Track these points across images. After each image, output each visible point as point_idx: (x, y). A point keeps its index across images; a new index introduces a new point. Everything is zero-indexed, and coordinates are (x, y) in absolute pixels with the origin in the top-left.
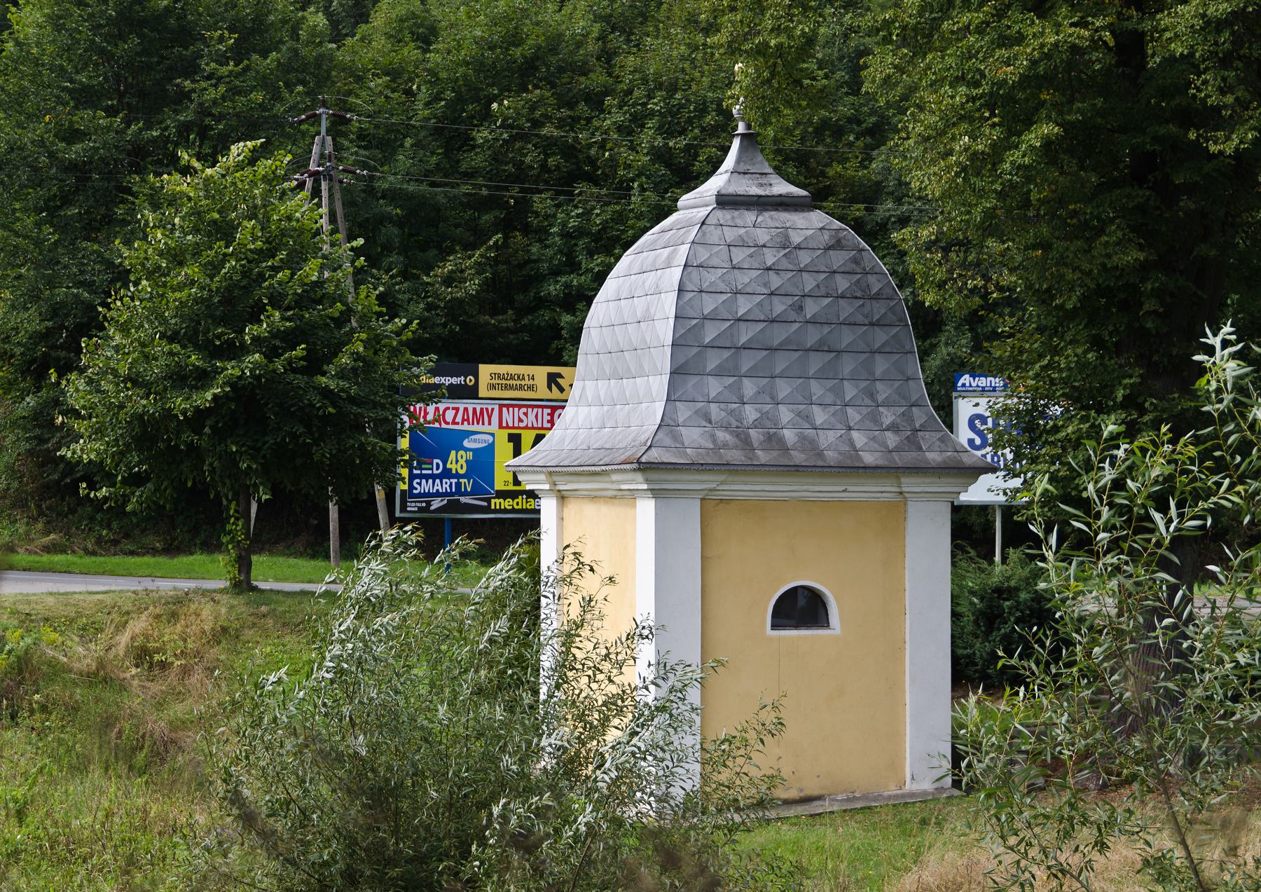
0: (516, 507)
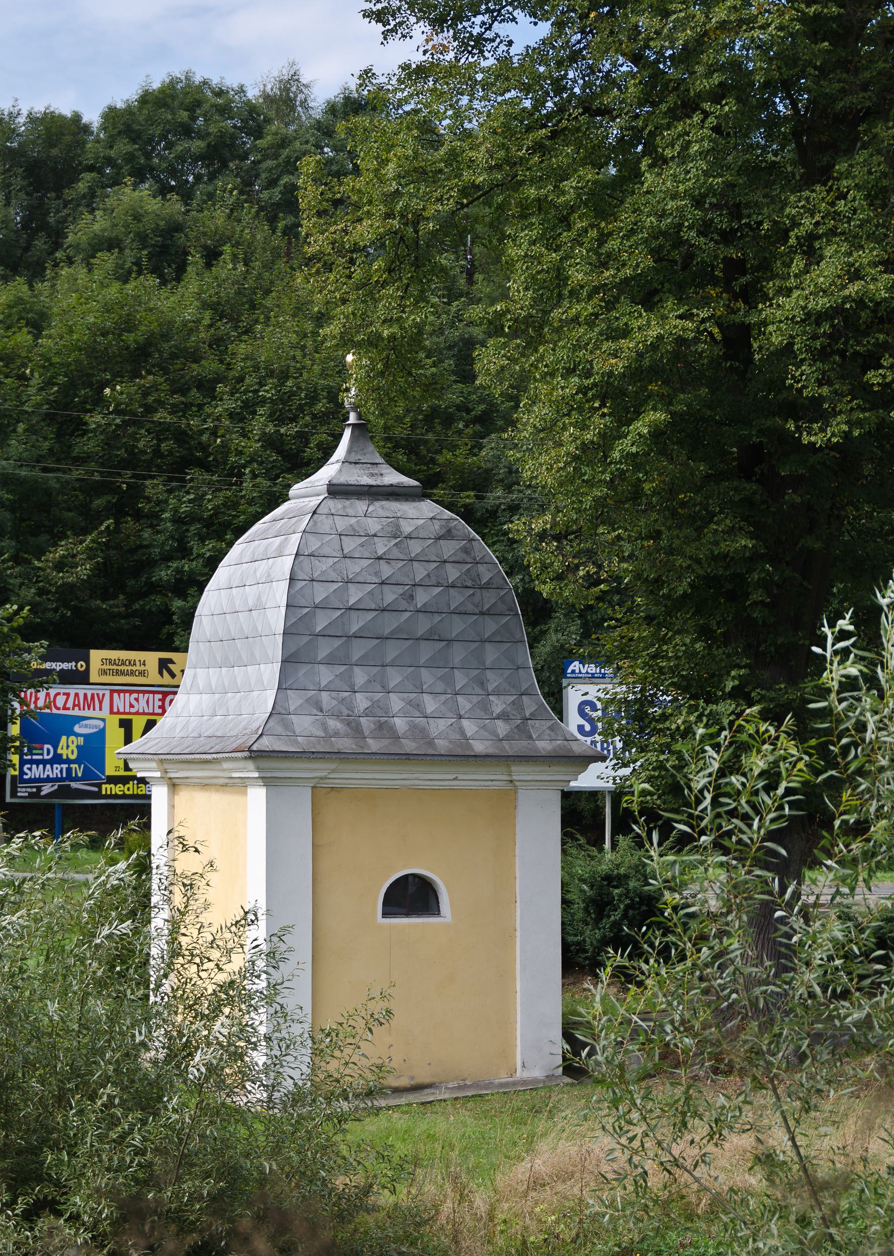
0: (127, 792)
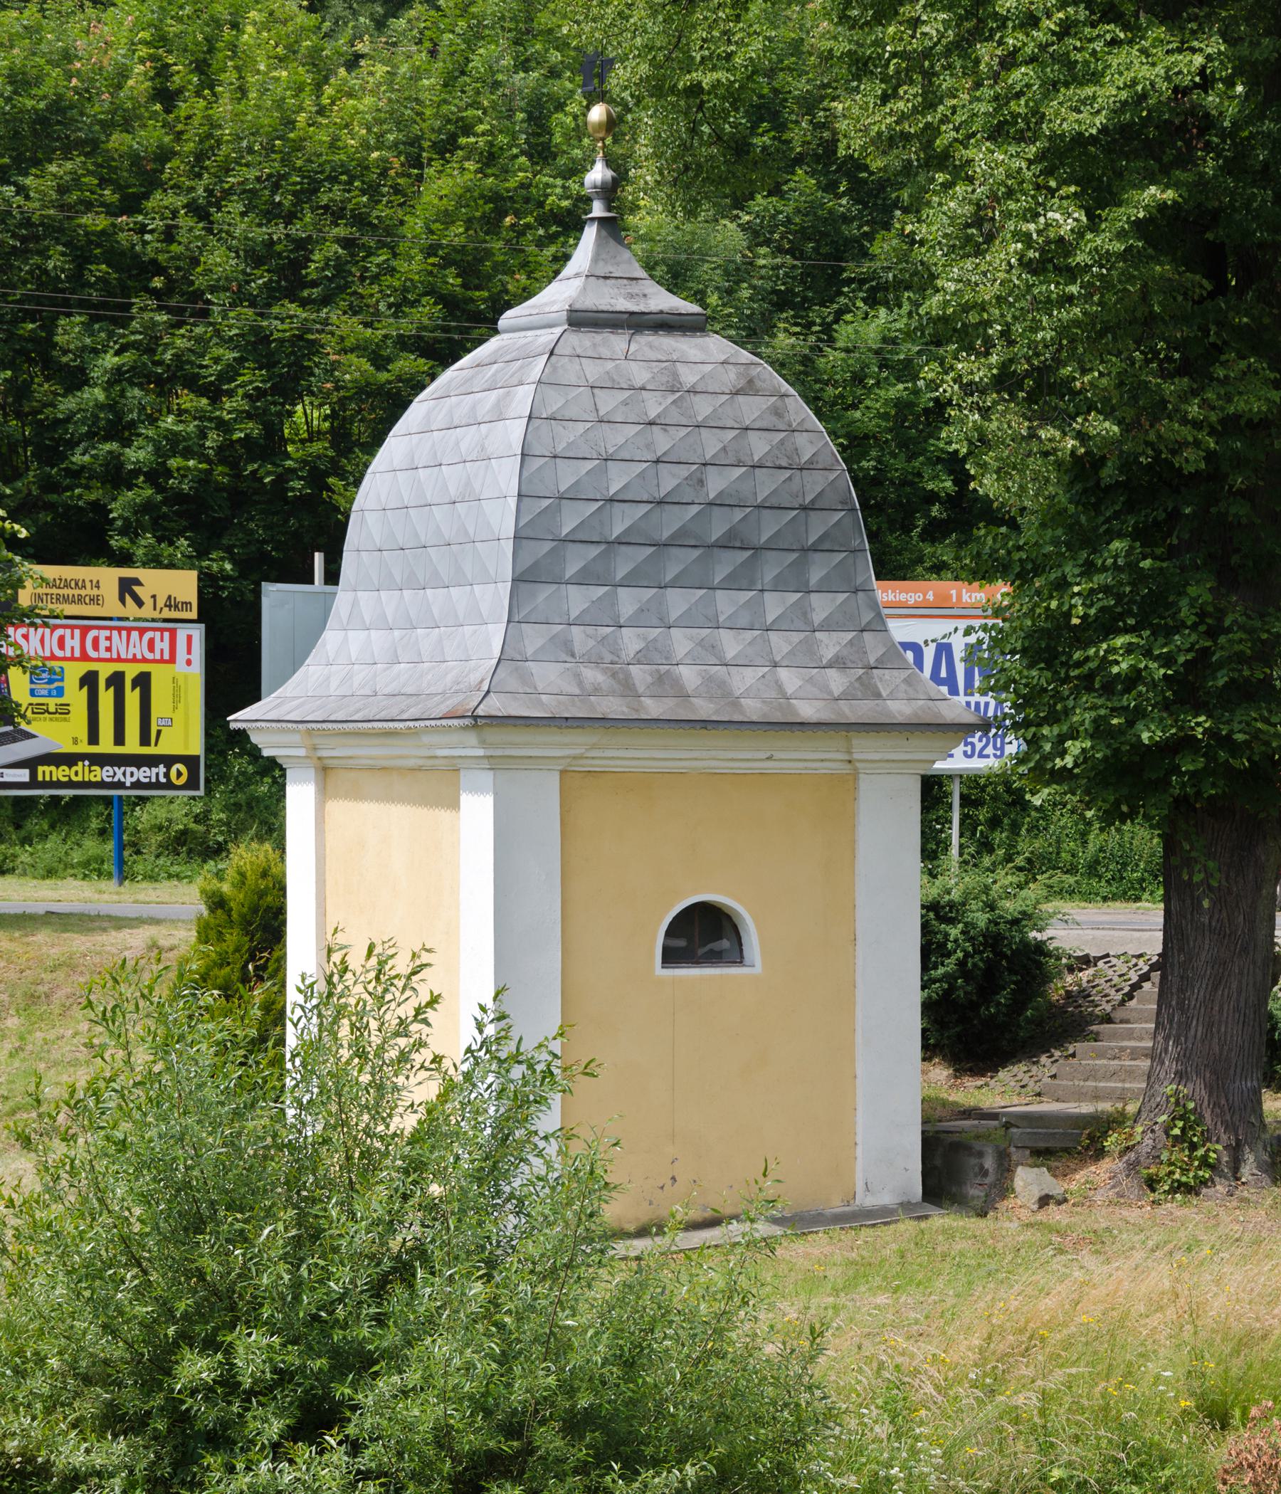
0: (74, 779)
